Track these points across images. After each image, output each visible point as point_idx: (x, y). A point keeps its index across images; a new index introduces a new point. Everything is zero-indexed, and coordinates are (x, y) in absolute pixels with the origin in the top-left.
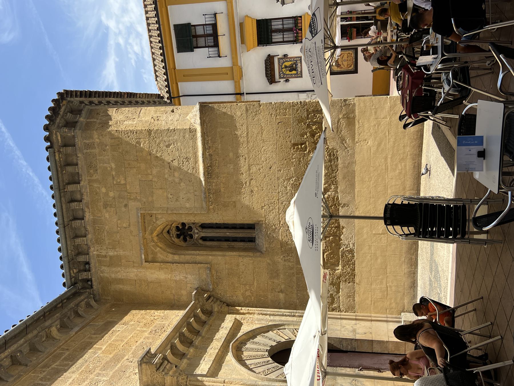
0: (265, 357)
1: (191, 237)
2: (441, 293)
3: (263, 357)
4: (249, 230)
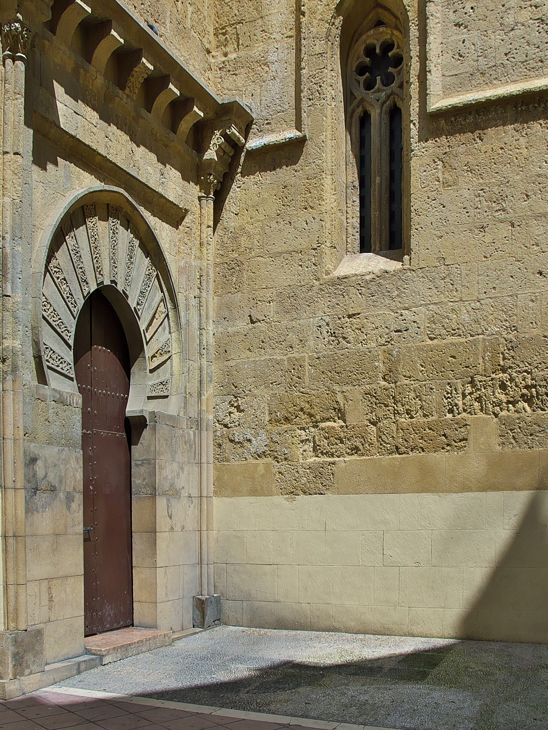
0: (98, 276)
1: (369, 86)
2: (248, 692)
3: (97, 270)
4: (388, 235)
